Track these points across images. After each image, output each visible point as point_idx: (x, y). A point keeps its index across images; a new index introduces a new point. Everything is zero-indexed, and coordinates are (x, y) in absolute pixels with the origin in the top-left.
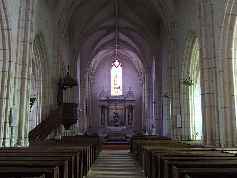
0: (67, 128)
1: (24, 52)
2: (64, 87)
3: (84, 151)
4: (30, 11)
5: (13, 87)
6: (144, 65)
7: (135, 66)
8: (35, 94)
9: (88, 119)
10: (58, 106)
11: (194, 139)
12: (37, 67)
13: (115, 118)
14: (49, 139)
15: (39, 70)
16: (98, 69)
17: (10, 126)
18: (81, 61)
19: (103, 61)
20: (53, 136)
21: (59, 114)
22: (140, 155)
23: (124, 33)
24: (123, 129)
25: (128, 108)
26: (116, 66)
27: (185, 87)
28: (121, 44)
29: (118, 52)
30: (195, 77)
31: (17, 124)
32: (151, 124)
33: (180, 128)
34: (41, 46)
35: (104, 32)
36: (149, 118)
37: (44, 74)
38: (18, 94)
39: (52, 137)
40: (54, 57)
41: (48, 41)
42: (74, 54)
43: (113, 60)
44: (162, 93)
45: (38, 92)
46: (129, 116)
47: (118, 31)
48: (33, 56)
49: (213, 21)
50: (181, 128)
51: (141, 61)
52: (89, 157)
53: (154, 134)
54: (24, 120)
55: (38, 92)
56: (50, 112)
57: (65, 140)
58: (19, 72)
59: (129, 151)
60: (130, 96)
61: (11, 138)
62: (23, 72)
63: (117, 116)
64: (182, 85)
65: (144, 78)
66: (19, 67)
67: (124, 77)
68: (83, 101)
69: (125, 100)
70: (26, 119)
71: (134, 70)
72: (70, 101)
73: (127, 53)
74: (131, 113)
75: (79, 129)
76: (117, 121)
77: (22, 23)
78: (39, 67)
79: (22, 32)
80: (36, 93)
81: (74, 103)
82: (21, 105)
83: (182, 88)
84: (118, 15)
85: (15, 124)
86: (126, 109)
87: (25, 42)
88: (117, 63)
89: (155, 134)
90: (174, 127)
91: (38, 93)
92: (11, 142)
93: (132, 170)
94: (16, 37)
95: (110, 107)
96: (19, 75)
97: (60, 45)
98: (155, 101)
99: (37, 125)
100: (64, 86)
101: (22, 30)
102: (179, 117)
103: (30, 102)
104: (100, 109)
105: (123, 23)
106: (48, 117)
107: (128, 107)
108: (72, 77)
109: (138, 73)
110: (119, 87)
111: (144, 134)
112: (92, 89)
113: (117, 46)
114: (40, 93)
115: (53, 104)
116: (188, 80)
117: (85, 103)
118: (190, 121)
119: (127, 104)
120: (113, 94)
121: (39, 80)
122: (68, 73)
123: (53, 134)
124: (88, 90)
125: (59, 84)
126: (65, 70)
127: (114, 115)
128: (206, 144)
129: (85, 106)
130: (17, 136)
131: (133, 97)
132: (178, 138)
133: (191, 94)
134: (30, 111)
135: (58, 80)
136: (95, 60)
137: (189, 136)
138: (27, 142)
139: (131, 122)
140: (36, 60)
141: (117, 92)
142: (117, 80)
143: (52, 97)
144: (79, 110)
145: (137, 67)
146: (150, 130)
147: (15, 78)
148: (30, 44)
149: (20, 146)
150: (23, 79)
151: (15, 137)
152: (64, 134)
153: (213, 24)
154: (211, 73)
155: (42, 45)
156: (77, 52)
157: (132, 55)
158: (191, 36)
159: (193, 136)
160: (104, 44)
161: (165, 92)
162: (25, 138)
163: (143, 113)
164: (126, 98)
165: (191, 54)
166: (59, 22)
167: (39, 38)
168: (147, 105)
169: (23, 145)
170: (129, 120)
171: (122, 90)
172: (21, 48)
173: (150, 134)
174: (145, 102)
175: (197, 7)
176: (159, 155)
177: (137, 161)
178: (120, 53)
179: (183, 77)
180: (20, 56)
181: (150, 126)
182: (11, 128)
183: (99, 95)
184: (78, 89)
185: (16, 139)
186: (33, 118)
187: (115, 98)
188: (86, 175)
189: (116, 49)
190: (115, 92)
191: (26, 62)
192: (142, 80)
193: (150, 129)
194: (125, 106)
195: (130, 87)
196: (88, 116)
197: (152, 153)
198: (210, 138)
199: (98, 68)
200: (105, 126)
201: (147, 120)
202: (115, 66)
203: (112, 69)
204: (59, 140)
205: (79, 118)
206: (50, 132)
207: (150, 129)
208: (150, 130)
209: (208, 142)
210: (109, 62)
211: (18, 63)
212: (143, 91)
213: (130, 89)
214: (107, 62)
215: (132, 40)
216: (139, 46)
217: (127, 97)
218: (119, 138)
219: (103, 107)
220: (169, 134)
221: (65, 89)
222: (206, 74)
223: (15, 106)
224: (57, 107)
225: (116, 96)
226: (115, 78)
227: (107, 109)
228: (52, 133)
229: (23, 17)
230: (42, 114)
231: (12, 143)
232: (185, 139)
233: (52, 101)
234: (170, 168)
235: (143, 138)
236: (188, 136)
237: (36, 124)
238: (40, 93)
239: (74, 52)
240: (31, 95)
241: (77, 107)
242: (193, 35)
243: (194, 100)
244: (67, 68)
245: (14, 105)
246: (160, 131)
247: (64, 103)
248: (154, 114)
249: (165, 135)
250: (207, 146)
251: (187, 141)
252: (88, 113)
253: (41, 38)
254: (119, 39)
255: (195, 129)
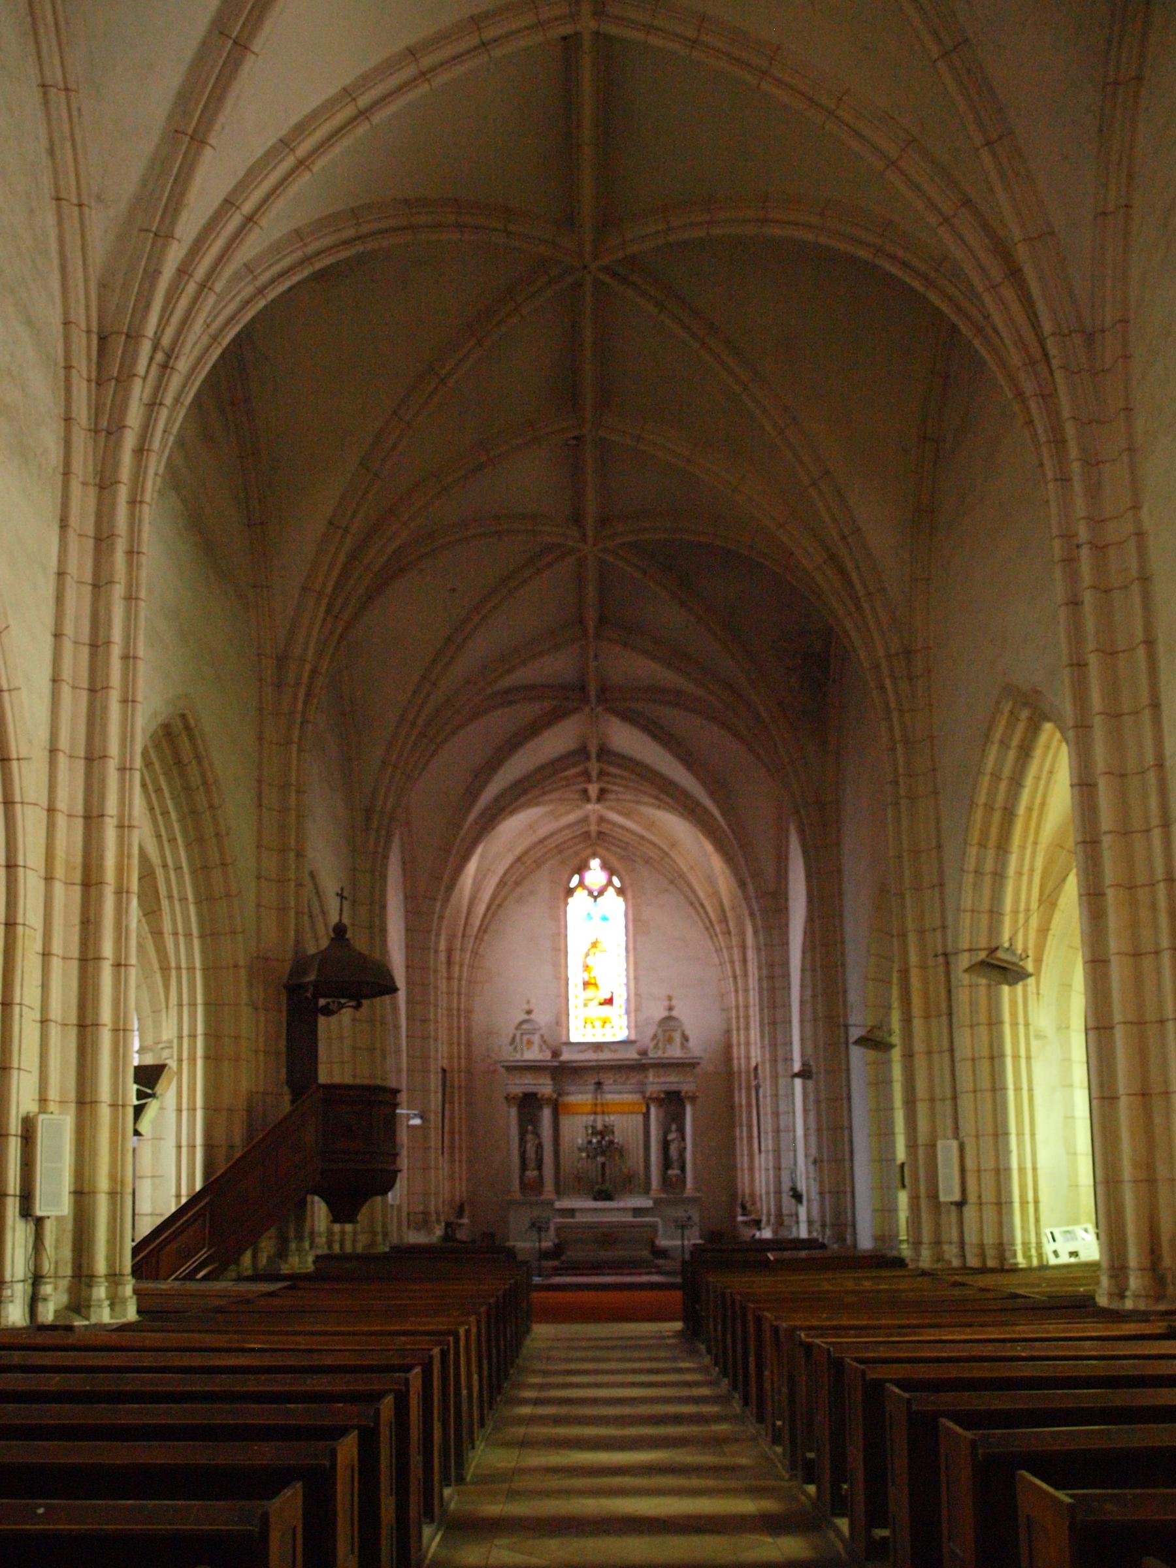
0: (342, 1212)
1: (92, 818)
2: (322, 1002)
3: (444, 1354)
4: (119, 590)
5: (37, 1005)
6: (742, 884)
7: (694, 892)
8: (165, 1038)
9: (452, 1161)
10: (293, 1102)
11: (1035, 1262)
12: (170, 897)
13: (595, 1157)
14: (250, 1272)
15: (181, 915)
16: (495, 907)
17: (26, 1212)
18: (408, 867)
19: (514, 883)
20: (269, 1258)
21: (304, 1140)
22: (752, 1359)
23: (629, 717)
24: (637, 1211)
25: (661, 1106)
26: (590, 893)
27: (983, 991)
28: (615, 776)
29: (602, 819)
30: (1032, 935)
31: (65, 1207)
32: (786, 1186)
33: (953, 1208)
34: (187, 789)
35: (528, 711)
36: (777, 1152)
37: (210, 936)
38: (63, 1046)
39: (263, 1260)
40: (259, 847)
41: (229, 764)
42: (368, 832)
43: (575, 862)
44: (846, 1026)
45: (180, 1029)
46: (665, 1145)
47: (599, 709)
48: (143, 834)
49: (1148, 627)
50: (960, 1205)
51: (729, 859)
52: (471, 1381)
53: (804, 1234)
54: (103, 1184)
55: (180, 1029)
56: (251, 1131)
57: (334, 1269)
58: (67, 925)
59: (678, 1325)
60: (670, 1040)
61: (37, 1279)
62: (89, 925)
63: (604, 1145)
64: (966, 979)
65: (743, 947)
66: (67, 898)
67: (635, 949)
68: (426, 1071)
69: (644, 1065)
70: (113, 1178)
71: (691, 910)
72: (354, 1076)
73: (651, 825)
74: (677, 1130)
75: (404, 1214)
76: (605, 1171)
77: (75, 662)
78: (183, 899)
79: (74, 704)
80: (168, 1032)
81: (378, 1082)
82: (85, 1102)
83: (962, 997)
84: (602, 621)
85: (53, 1200)
86: (653, 1110)
87: (93, 758)
88: (595, 875)
89: (810, 1232)
90: (924, 1204)
91: (180, 1037)
92: (34, 1301)
93: (716, 1442)
94: (42, 734)
95: (571, 1099)
96: (65, 940)
97: (293, 780)
98: (804, 1064)
99: (184, 1200)
100: (317, 995)
101: (75, 699)
102: (947, 1149)
103: (135, 1087)
104: (514, 1112)
105: (632, 666)
106: (242, 1157)
107: (663, 1099)
108: (367, 953)
109: (709, 927)
110: (608, 997)
111: (747, 1233)
112: (469, 1011)
113: (593, 789)
114: (193, 1036)
115: (265, 1093)
116: (1000, 954)
117: (435, 1081)
118: (1008, 1169)
119: (655, 1083)
120: (579, 1033)
121: (184, 965)
122: (340, 931)
123: (267, 1245)
124: (450, 1016)
125: (293, 989)
126: (324, 913)
127: (590, 1142)
128: (1122, 1297)
129: (435, 1100)
130: (70, 1266)
131: (683, 1046)
132: (947, 1256)
133: (1015, 1024)
134: (137, 1133)
135: (288, 967)
136: (480, 862)
137: (1003, 1248)
138: (124, 1301)
139: (676, 1172)
140: (163, 856)
141: (598, 1024)
142: (593, 964)
143: (256, 1052)
144: (409, 1118)
145: (701, 895)
146: (780, 1215)
147: (46, 955)
148: (122, 769)
149: (88, 1319)
150: (88, 960)
151: (56, 1272)
152: (330, 1244)
153: (1150, 643)
154: (1144, 914)
155: (195, 780)
156: (386, 821)
157: (676, 828)
158: (1013, 717)
159: (1026, 1245)
160: (528, 777)
161: (858, 1022)
162: (114, 1277)
163: (741, 1126)
164: (651, 1055)
165: (1009, 813)
166: (282, 660)
167: (176, 747)
168: (766, 1089)
169: (104, 1316)
170: (667, 1163)
171: (628, 1012)
172: (70, 794)
173: (784, 1234)
174: (748, 1072)
175: (1058, 554)
176: (852, 1359)
177: (724, 1373)
178: (614, 824)
179: (968, 936)
180: (69, 836)
181: (778, 1192)
182: (31, 1226)
183: (507, 1040)
184: (395, 1009)
185: (64, 1284)
186: (165, 1166)
187: (590, 1056)
188: (461, 1479)
189: (588, 800)
190: (589, 1026)
191: (101, 867)
192: (732, 962)
193: (779, 1208)
194: (642, 1092)
195: (670, 998)
196: (452, 1148)
197: (838, 1365)
198: (1147, 1263)
199: (497, 902)
200: (543, 1197)
201: (763, 1161)
202: (586, 892)
203: (569, 908)
204: (306, 1277)
205: (404, 1162)
206: (251, 1240)
207: (779, 1208)
208: (780, 1215)
209: (1134, 1282)
210: (563, 860)
211: (59, 872)
212: (738, 1018)
213: (671, 1008)
214: (547, 866)
215: (677, 756)
216: (717, 785)
217: (656, 1046)
218: (618, 1253)
219: (528, 1104)
220: (886, 1237)
221: (328, 1012)
222: (1114, 920)
223: (52, 1107)
224: (286, 1106)
225: (598, 1046)
226: (587, 955)
227: (547, 1113)
228: (263, 1245)
229: (77, 625)
230: (209, 1147)
231: (41, 1307)
232: (984, 1261)
233: (254, 1075)
234: (924, 1428)
235: (754, 1257)
236: (1001, 1244)
237: (178, 1196)
238: (193, 1036)
239: (368, 819)
240: (171, 1047)
241: (396, 1105)
242: (1034, 711)
243: (1028, 1058)
244: (333, 904)
245: (43, 1100)
246: (840, 1220)
247: (324, 1086)
248: (800, 1132)
249: (865, 1242)
250: (1129, 1304)
251: (993, 1270)
252: (452, 1119)
253: (186, 739)
254: (605, 753)
255: (1037, 1210)
